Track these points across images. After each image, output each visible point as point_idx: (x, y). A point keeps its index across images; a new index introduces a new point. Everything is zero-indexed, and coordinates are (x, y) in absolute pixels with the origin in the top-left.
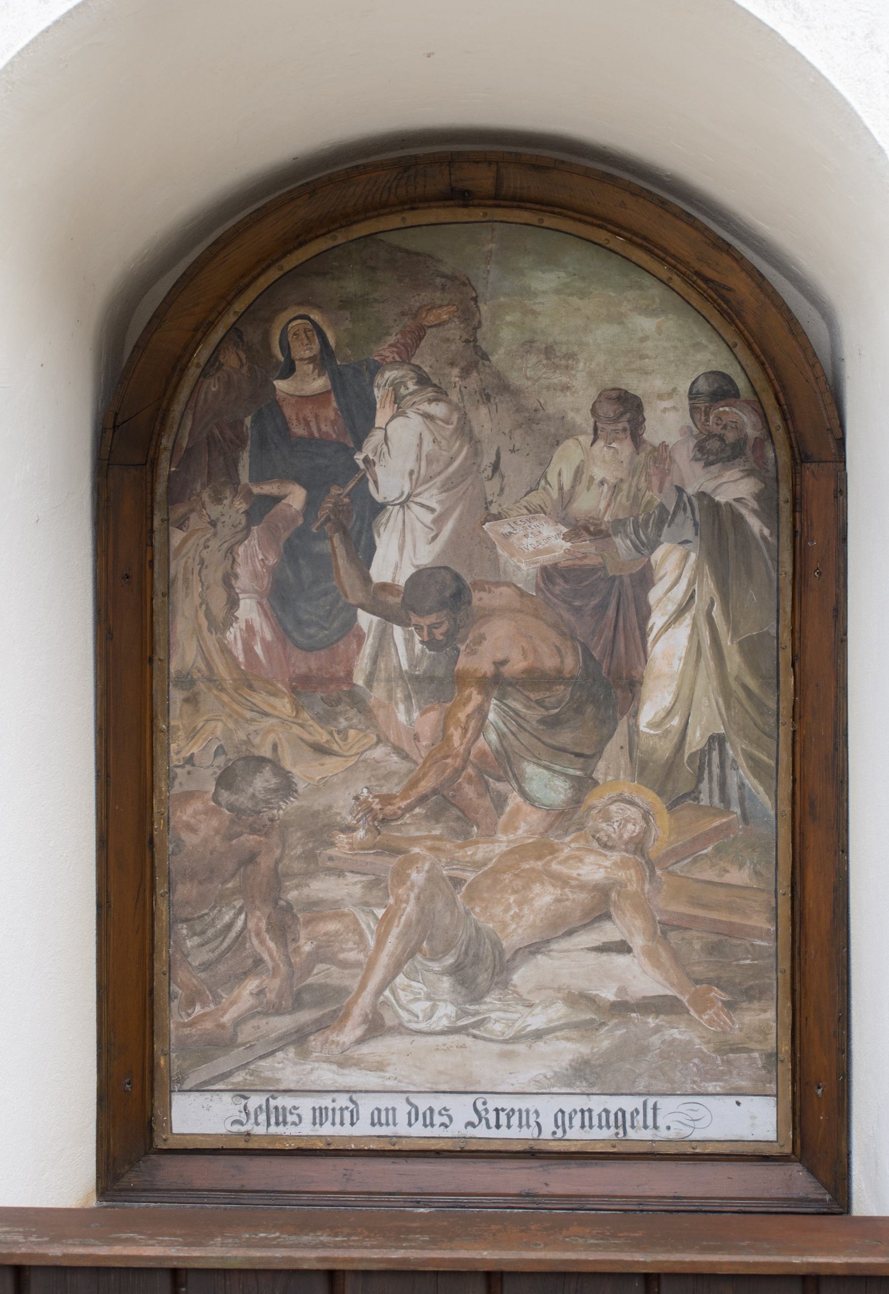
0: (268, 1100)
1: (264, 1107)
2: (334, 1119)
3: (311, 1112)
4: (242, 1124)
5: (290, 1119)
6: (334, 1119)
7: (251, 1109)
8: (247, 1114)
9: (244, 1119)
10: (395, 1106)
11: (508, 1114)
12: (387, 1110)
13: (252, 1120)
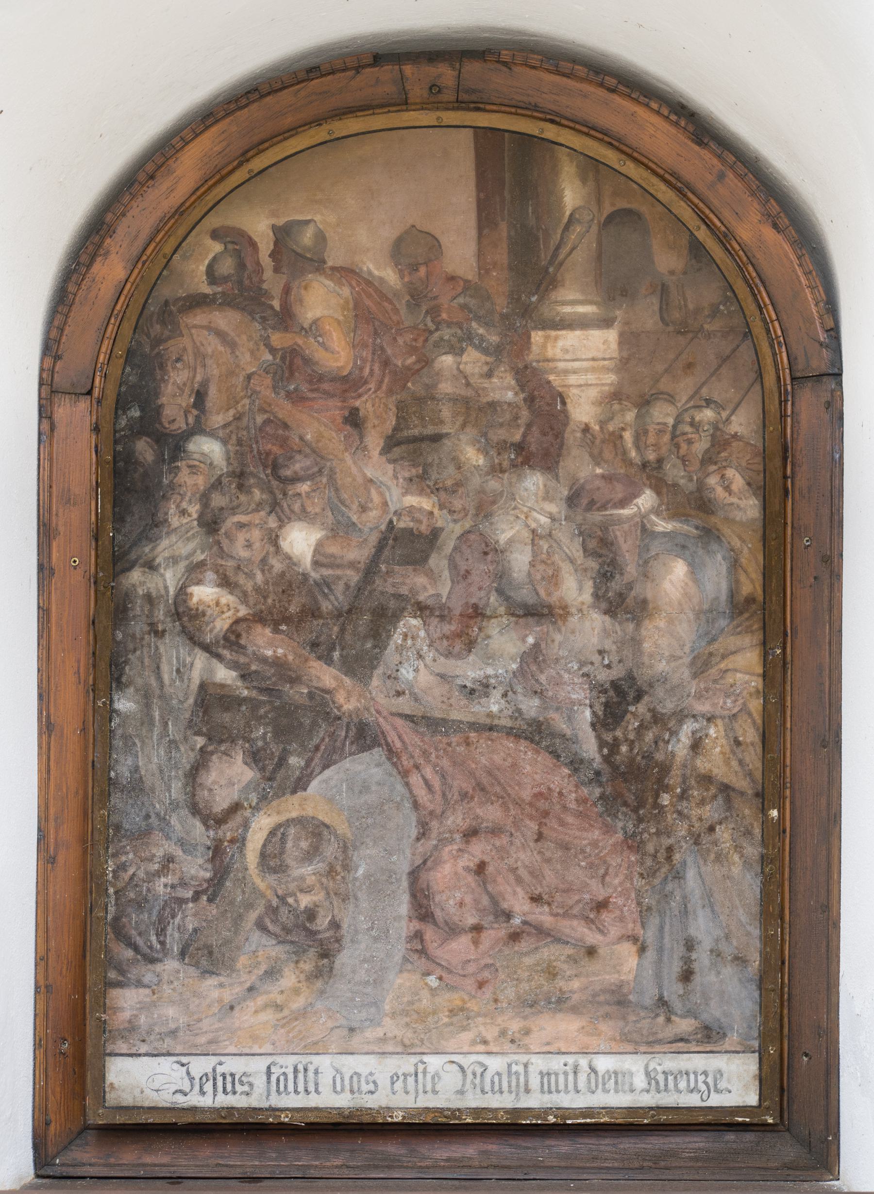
5: (239, 1088)
7: (196, 1073)
8: (192, 1079)
9: (186, 1087)
11: (676, 1078)
13: (197, 1088)
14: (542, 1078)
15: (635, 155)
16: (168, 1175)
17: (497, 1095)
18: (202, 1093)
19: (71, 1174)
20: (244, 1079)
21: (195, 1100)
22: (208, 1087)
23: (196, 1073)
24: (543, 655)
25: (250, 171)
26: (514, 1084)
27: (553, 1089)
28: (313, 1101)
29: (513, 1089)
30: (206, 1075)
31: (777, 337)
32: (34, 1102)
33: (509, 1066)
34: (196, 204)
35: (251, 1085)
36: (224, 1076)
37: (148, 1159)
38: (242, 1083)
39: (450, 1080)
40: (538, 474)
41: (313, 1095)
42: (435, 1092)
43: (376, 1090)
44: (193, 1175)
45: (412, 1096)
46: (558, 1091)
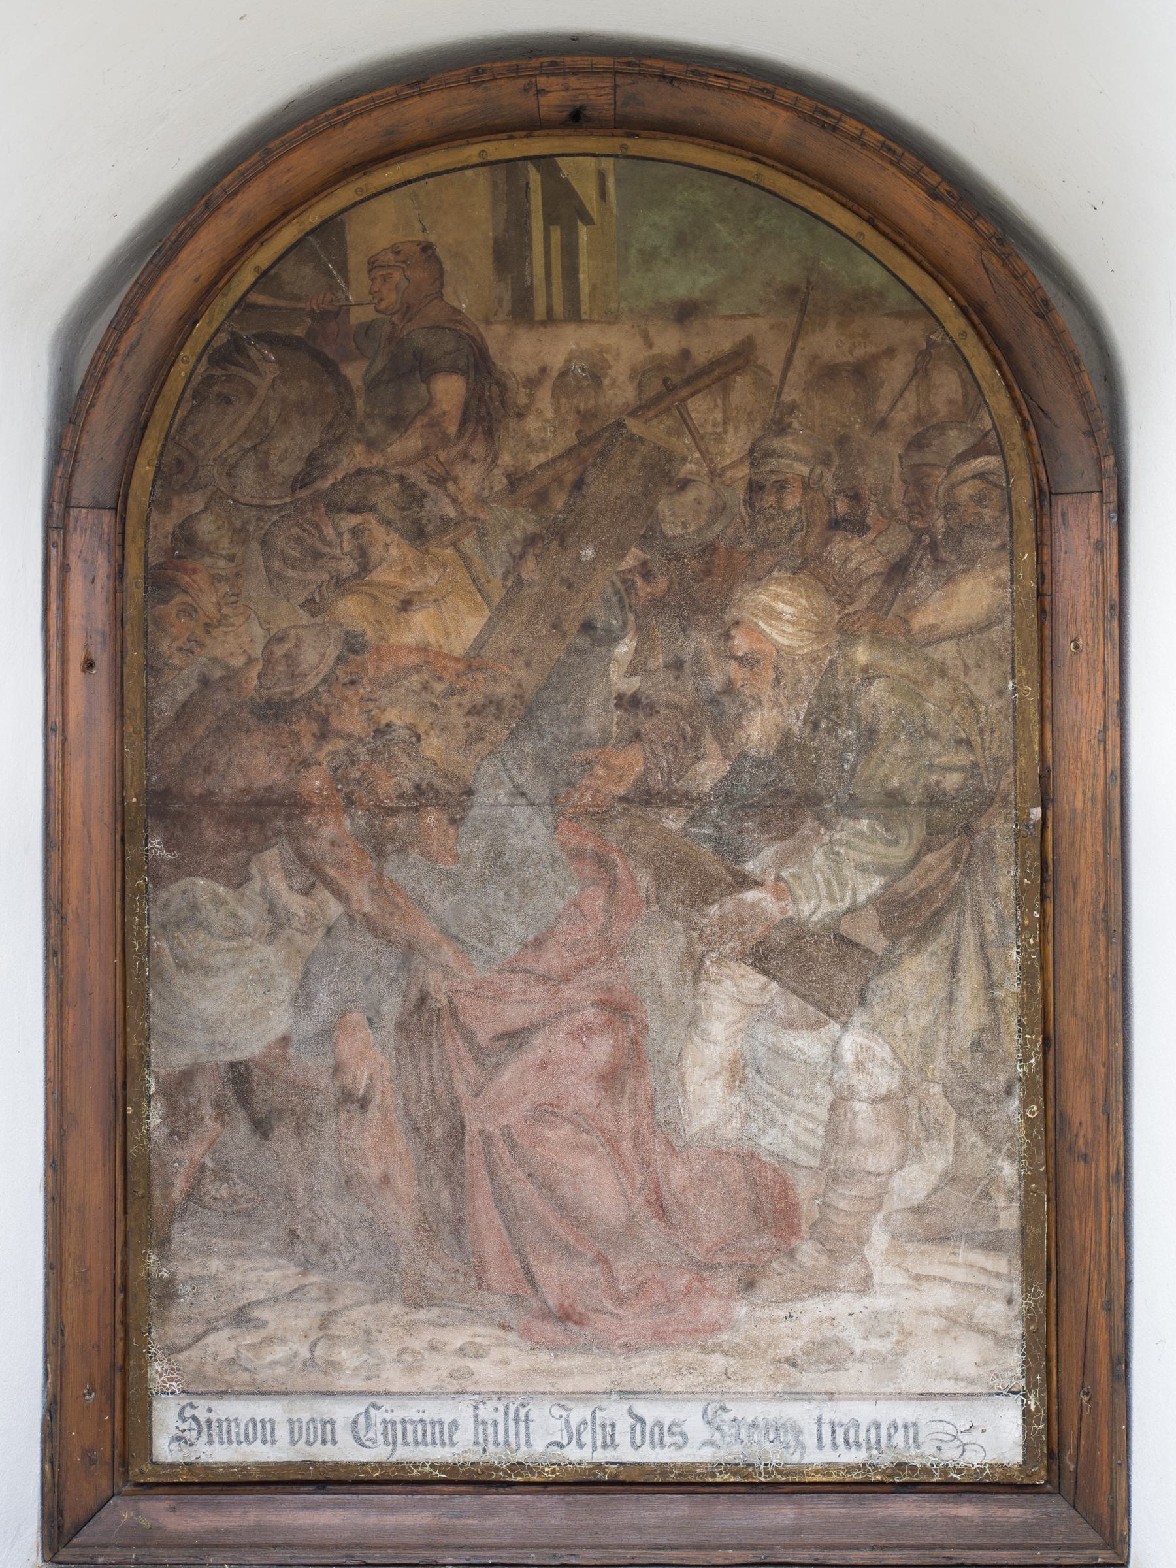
2: (264, 1436)
3: (287, 1426)
4: (562, 1447)
5: (667, 1439)
6: (264, 1436)
10: (274, 1417)
15: (119, 886)
16: (754, 1560)
17: (439, 1447)
18: (581, 1445)
20: (676, 1429)
21: (573, 1454)
22: (587, 1438)
26: (437, 1435)
28: (610, 1455)
30: (585, 1422)
31: (306, 130)
32: (1128, 1477)
33: (593, 1413)
34: (118, 688)
36: (604, 1425)
38: (672, 1434)
39: (697, 1428)
41: (329, 1445)
42: (453, 1444)
43: (685, 1443)
45: (588, 1448)
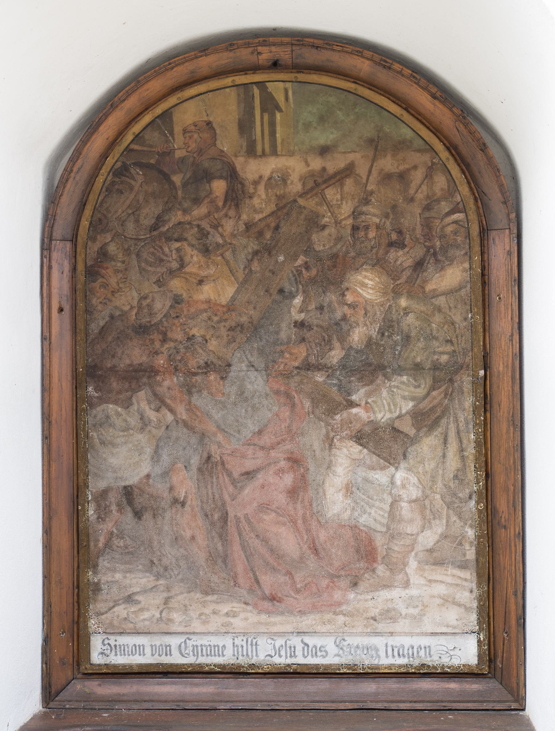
0: (286, 642)
1: (284, 645)
4: (272, 657)
5: (319, 654)
12: (139, 646)
13: (277, 655)
14: (152, 648)
17: (217, 657)
18: (280, 656)
19: (458, 708)
20: (322, 649)
22: (283, 653)
23: (278, 645)
24: (119, 392)
25: (179, 98)
27: (217, 654)
29: (196, 654)
35: (326, 652)
36: (290, 647)
37: (196, 690)
38: (321, 651)
40: (347, 180)
42: (223, 656)
43: (327, 655)
44: (420, 708)
46: (215, 655)
